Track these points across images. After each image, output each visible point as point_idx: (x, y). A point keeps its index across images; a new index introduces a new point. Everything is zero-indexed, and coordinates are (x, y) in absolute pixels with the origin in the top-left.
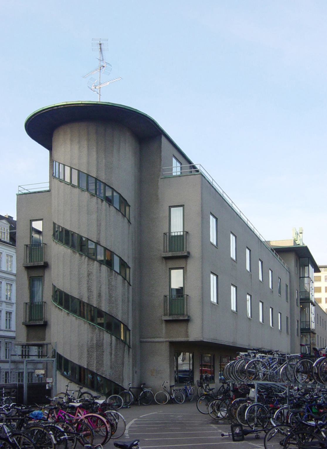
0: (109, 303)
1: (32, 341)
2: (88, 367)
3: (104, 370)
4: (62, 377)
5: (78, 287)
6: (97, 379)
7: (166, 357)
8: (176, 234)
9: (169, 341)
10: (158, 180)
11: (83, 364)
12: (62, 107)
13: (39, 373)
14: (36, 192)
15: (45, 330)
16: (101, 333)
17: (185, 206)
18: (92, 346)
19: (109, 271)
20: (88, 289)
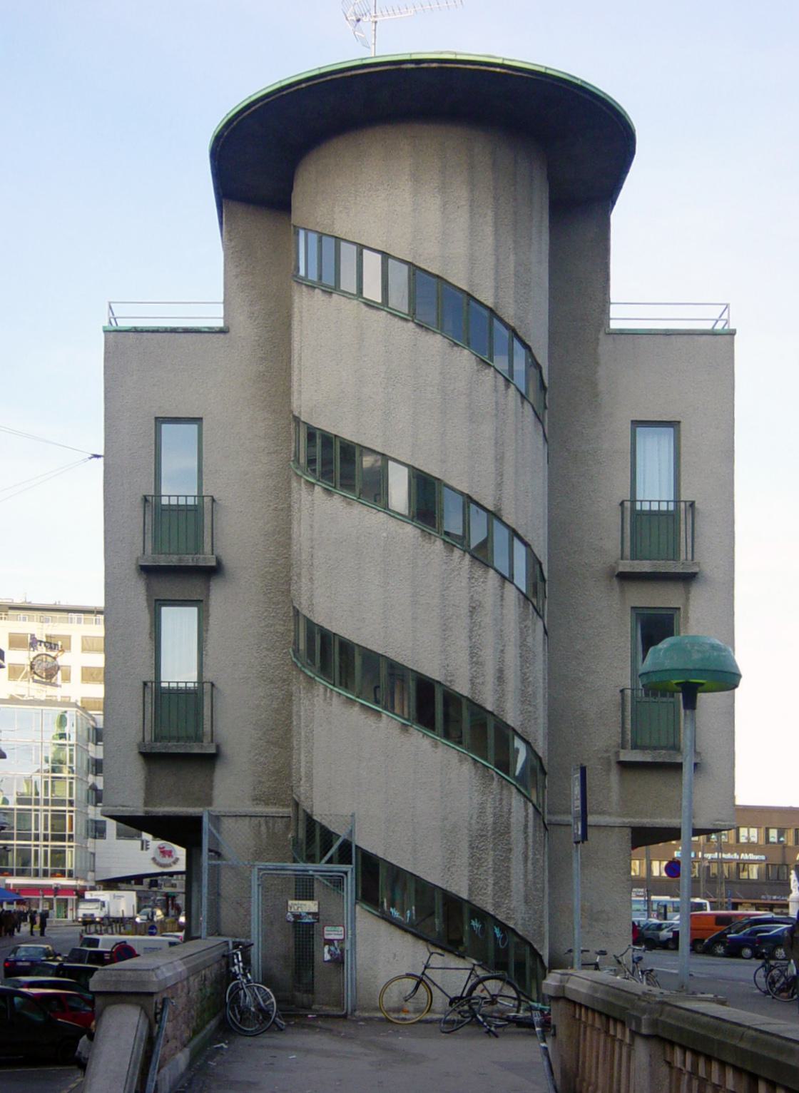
0: (523, 702)
1: (164, 806)
2: (470, 895)
3: (512, 906)
4: (383, 927)
5: (442, 646)
6: (495, 934)
7: (622, 872)
8: (174, 501)
9: (633, 826)
10: (598, 339)
11: (457, 888)
12: (434, 65)
13: (300, 910)
14: (178, 328)
15: (214, 768)
16: (504, 792)
17: (204, 421)
18: (482, 830)
19: (522, 604)
20: (472, 655)
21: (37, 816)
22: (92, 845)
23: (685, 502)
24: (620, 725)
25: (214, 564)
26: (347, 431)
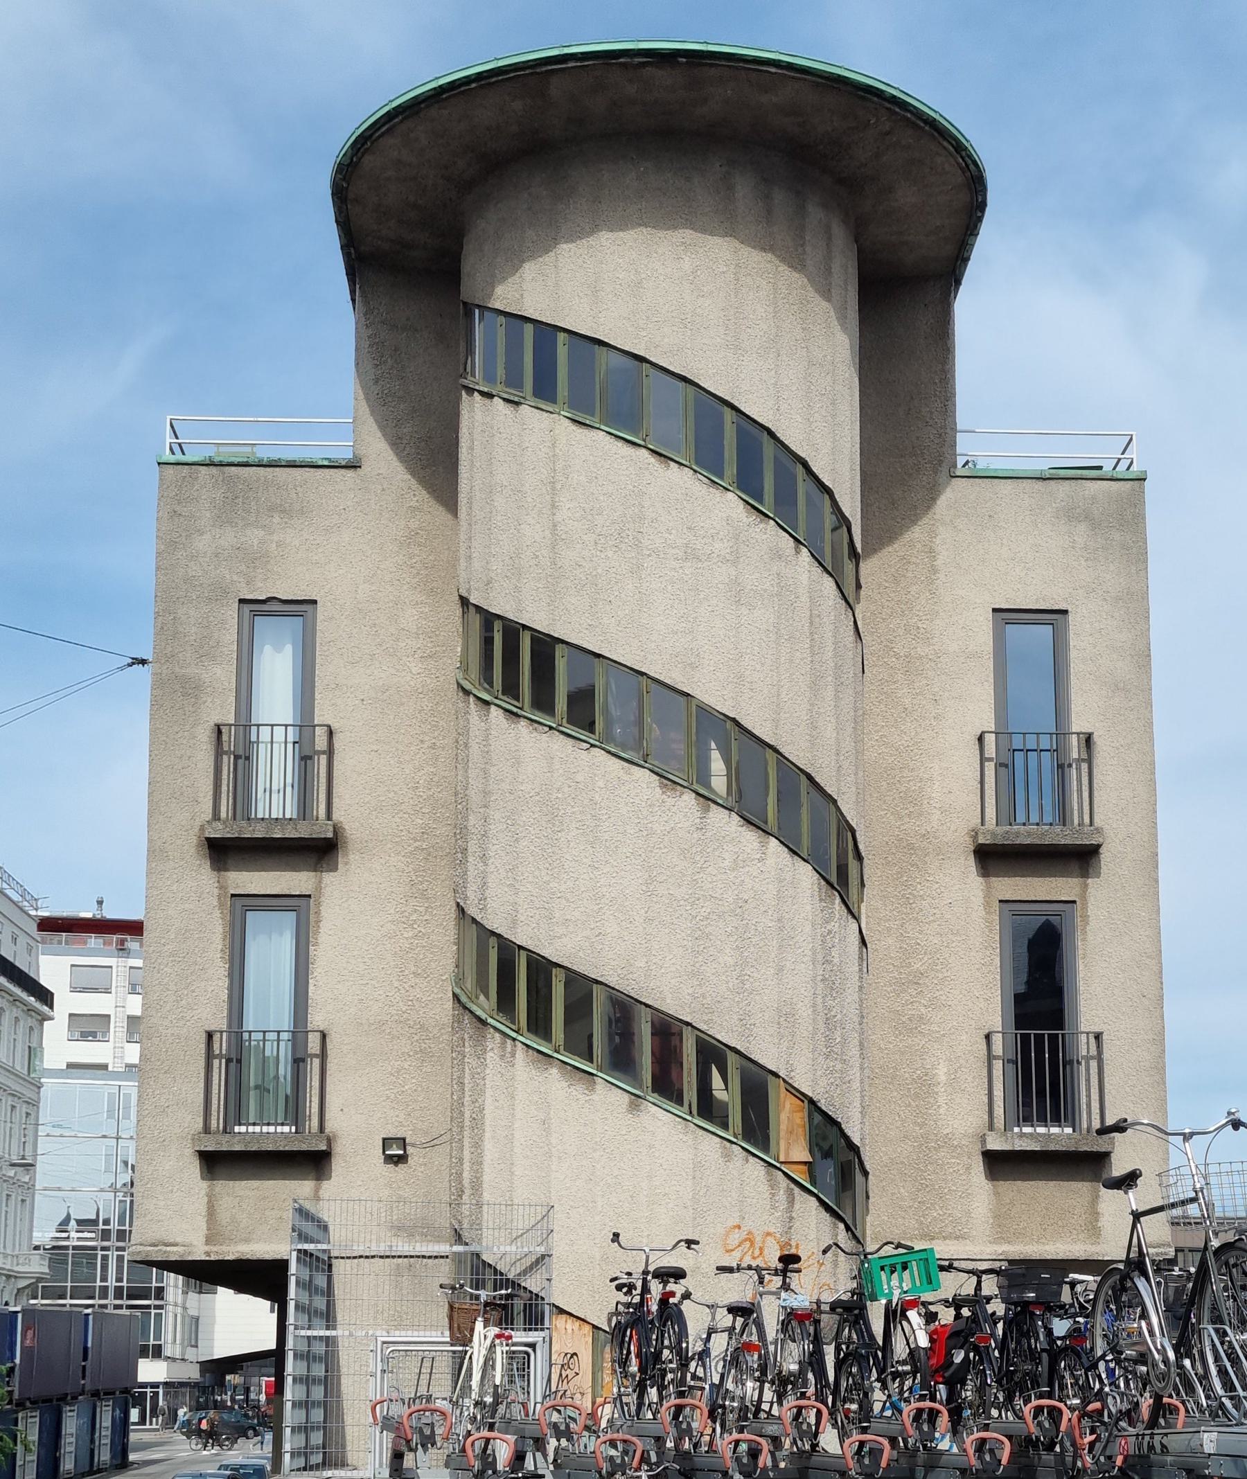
21: (105, 1258)
22: (195, 1304)
23: (1078, 734)
24: (987, 1092)
25: (330, 835)
26: (537, 617)
